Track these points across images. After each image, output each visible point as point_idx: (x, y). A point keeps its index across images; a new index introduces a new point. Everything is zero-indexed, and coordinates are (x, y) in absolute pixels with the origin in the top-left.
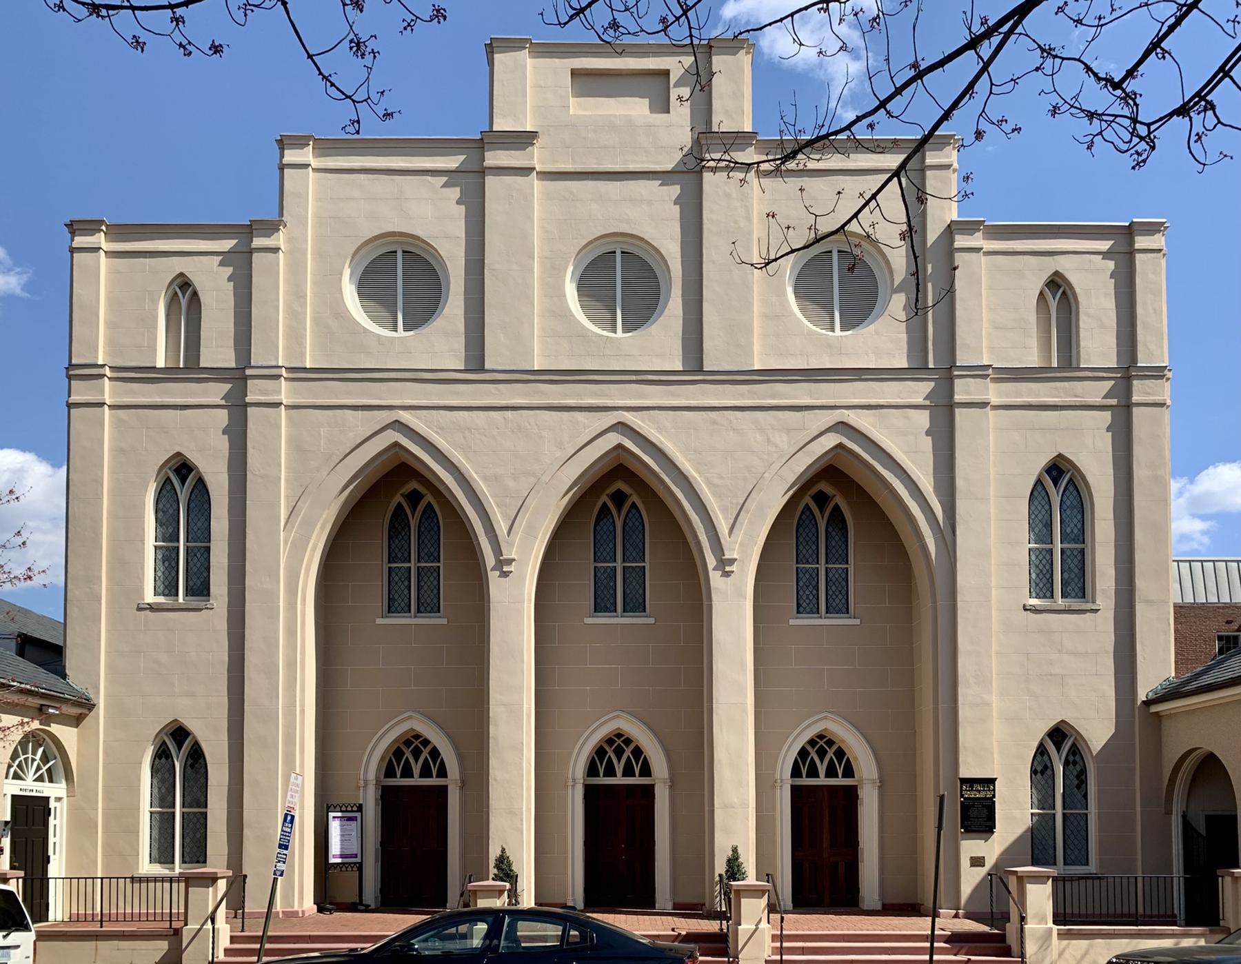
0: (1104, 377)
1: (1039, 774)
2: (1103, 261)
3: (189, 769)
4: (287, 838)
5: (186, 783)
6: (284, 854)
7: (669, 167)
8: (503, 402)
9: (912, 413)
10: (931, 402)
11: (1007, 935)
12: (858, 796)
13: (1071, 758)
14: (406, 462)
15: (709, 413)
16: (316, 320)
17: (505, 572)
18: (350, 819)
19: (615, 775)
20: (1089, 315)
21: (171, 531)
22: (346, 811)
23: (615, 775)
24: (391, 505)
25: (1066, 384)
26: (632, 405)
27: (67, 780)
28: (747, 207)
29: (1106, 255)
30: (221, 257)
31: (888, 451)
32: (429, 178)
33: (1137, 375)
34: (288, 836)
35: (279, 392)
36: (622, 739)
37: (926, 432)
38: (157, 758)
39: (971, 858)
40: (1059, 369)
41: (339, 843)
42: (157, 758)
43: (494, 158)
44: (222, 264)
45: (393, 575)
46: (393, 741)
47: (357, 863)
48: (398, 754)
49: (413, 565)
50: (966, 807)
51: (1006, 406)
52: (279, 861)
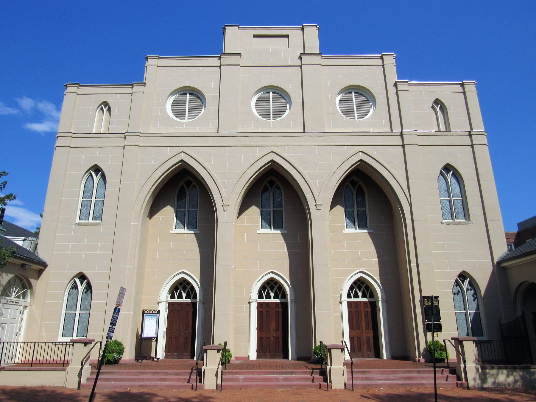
3: (84, 293)
4: (115, 320)
5: (82, 300)
6: (113, 328)
11: (456, 370)
12: (376, 306)
14: (186, 168)
21: (89, 194)
34: (116, 319)
36: (273, 282)
38: (71, 289)
42: (71, 289)
45: (178, 213)
47: (155, 338)
49: (186, 209)
52: (110, 332)
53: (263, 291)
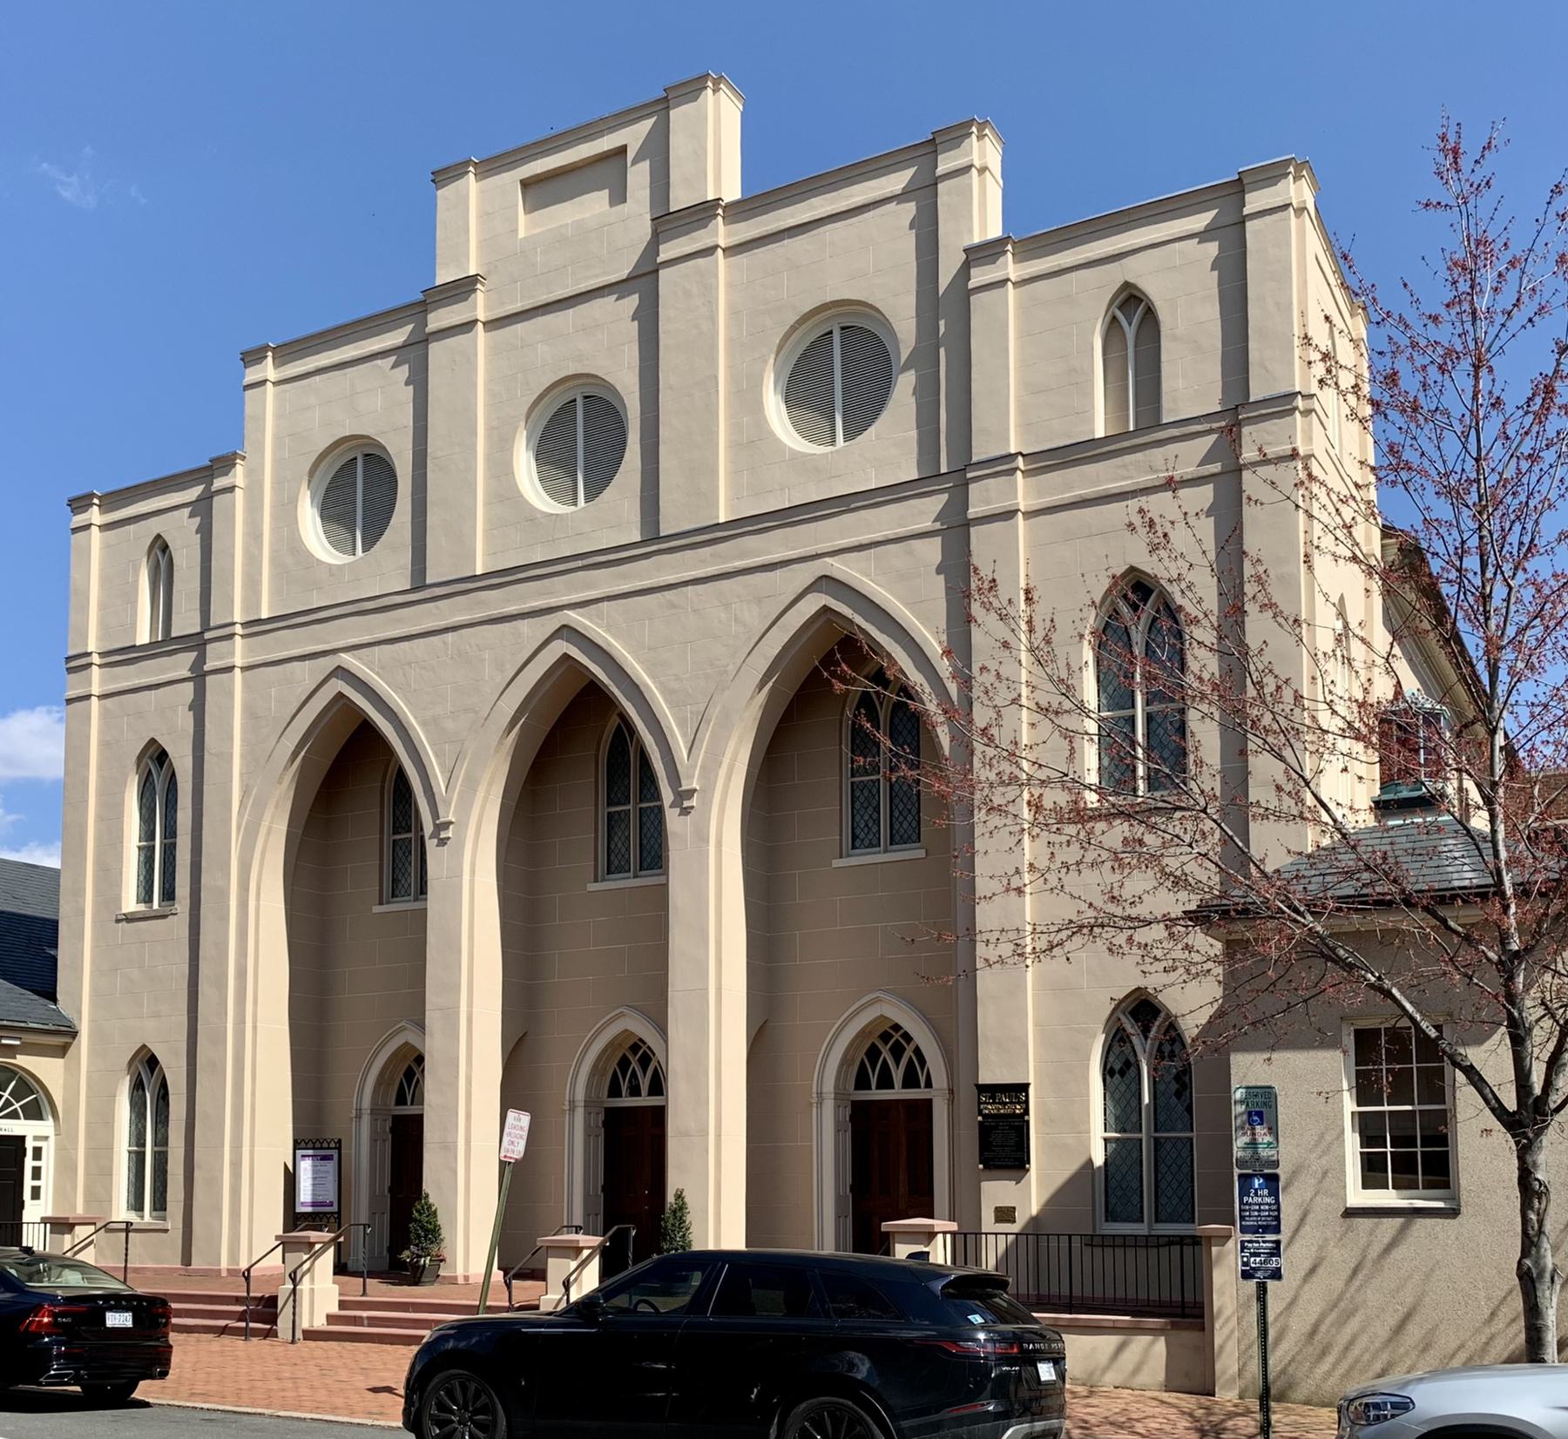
0: (1199, 432)
1: (1117, 1076)
2: (1200, 246)
7: (624, 274)
8: (442, 624)
9: (916, 544)
10: (942, 525)
13: (1167, 1048)
15: (666, 593)
16: (274, 561)
17: (442, 839)
18: (324, 1158)
19: (891, 1086)
20: (1175, 338)
22: (321, 1148)
23: (891, 1086)
24: (608, 728)
25: (1139, 456)
26: (578, 601)
27: (53, 1117)
28: (710, 302)
29: (1203, 236)
30: (190, 509)
31: (883, 607)
32: (379, 362)
33: (1249, 418)
35: (232, 654)
37: (937, 569)
39: (996, 1208)
40: (1139, 430)
41: (310, 1188)
43: (439, 319)
44: (191, 516)
45: (398, 848)
46: (857, 1036)
47: (335, 1213)
48: (873, 1053)
50: (988, 1129)
51: (1048, 508)
53: (14, 1082)
